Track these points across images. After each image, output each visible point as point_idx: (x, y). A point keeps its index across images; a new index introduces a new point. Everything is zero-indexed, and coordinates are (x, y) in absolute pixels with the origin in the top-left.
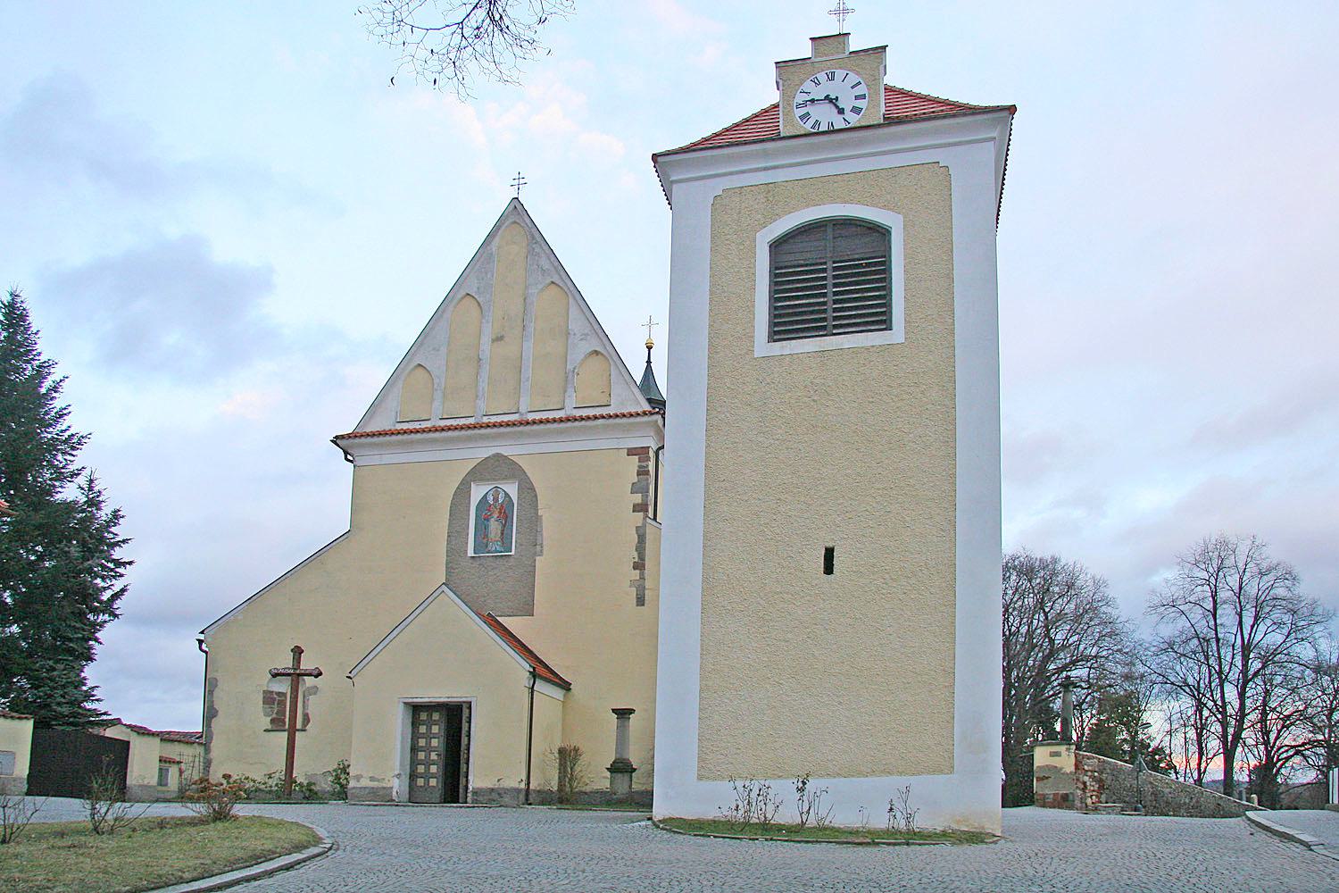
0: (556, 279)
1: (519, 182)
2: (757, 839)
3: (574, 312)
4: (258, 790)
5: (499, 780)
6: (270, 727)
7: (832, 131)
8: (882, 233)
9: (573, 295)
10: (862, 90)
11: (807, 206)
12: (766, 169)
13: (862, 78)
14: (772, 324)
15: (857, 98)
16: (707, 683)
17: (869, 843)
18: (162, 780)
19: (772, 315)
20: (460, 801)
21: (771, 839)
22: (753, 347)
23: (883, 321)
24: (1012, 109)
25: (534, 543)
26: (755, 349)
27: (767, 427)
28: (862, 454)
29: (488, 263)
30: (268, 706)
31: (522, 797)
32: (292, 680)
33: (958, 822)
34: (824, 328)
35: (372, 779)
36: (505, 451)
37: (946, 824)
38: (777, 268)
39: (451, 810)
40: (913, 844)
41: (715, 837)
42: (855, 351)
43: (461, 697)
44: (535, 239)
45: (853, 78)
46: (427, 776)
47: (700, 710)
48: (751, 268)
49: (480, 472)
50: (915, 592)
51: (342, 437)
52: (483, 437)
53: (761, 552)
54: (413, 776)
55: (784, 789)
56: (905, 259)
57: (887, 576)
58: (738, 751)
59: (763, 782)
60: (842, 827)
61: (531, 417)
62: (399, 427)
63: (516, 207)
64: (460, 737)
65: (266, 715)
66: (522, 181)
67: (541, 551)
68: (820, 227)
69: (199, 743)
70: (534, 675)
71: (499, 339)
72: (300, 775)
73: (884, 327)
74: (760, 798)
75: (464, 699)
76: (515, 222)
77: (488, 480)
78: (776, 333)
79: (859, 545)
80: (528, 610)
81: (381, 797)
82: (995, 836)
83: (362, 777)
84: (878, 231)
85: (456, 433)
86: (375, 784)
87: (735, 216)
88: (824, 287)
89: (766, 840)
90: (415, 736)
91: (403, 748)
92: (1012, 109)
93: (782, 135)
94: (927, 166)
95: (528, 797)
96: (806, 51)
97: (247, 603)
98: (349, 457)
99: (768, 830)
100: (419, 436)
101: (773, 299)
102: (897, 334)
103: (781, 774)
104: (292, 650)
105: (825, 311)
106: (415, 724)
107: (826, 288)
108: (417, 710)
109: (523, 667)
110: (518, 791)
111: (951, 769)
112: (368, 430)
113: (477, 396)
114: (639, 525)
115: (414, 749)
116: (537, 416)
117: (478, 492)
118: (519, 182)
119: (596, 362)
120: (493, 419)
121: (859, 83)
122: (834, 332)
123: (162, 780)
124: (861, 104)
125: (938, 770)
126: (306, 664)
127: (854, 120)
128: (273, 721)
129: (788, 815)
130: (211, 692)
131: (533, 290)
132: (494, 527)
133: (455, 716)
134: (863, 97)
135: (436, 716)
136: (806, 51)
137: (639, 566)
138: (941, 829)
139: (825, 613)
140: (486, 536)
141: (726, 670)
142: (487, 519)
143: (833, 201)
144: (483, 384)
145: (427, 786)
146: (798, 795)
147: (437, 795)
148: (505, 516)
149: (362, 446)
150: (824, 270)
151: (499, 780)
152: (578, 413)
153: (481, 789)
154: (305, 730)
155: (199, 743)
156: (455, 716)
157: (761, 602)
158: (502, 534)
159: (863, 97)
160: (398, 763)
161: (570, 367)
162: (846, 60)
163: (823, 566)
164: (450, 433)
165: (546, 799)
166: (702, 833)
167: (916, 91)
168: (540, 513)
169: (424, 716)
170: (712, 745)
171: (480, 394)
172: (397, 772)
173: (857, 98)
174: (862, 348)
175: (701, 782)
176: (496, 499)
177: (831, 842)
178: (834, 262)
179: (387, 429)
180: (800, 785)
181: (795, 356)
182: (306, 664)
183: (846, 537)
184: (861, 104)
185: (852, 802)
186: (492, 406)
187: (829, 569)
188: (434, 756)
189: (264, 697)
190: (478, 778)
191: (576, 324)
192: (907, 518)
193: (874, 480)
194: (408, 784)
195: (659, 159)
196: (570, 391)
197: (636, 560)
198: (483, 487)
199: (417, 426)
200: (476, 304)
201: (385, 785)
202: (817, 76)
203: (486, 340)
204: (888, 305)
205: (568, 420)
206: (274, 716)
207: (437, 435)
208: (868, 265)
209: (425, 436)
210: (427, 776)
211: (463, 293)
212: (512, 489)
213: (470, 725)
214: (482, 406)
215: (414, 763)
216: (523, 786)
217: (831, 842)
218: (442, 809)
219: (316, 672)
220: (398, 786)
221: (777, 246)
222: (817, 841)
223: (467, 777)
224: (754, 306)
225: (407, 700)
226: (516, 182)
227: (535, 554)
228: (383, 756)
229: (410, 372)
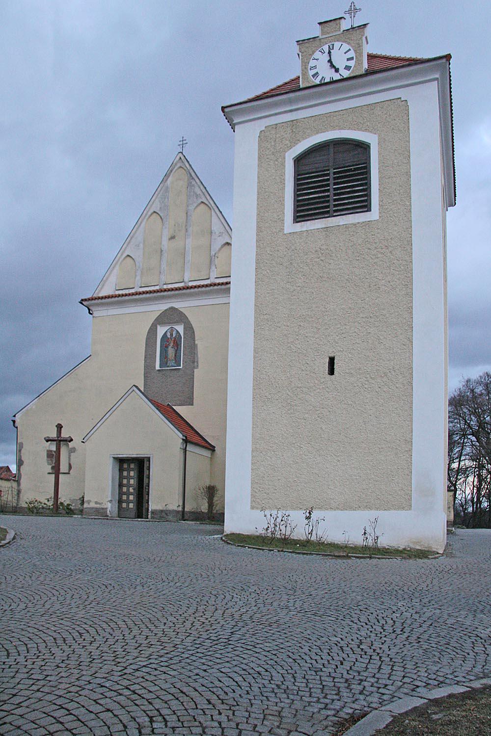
2: (273, 550)
3: (215, 219)
4: (43, 508)
5: (166, 505)
6: (51, 471)
7: (333, 82)
8: (363, 148)
9: (214, 210)
10: (352, 54)
11: (317, 133)
12: (291, 111)
13: (352, 47)
14: (296, 211)
15: (348, 60)
16: (256, 446)
17: (344, 556)
18: (452, 491)
19: (296, 206)
20: (144, 516)
21: (282, 551)
22: (284, 226)
23: (366, 206)
24: (448, 57)
25: (193, 362)
26: (285, 228)
27: (293, 278)
28: (352, 294)
29: (166, 193)
30: (49, 459)
31: (180, 516)
32: (57, 444)
33: (414, 543)
34: (328, 212)
35: (96, 503)
36: (176, 305)
37: (406, 544)
38: (299, 175)
39: (139, 523)
40: (374, 558)
41: (249, 547)
42: (346, 226)
43: (144, 455)
44: (192, 176)
45: (346, 47)
46: (128, 502)
47: (252, 464)
49: (162, 319)
50: (386, 387)
51: (86, 300)
52: (163, 297)
54: (120, 501)
55: (297, 517)
56: (379, 164)
57: (368, 376)
58: (275, 491)
59: (284, 512)
60: (339, 543)
61: (191, 284)
62: (117, 293)
63: (183, 159)
64: (143, 478)
65: (49, 464)
66: (184, 142)
67: (198, 366)
68: (325, 146)
69: (14, 480)
70: (186, 441)
71: (173, 238)
72: (64, 498)
73: (366, 210)
74: (282, 523)
75: (146, 456)
76: (181, 167)
77: (165, 323)
78: (298, 217)
79: (350, 355)
80: (189, 401)
81: (101, 513)
82: (438, 553)
83: (91, 501)
84: (362, 147)
85: (148, 295)
86: (98, 506)
87: (273, 144)
88: (328, 185)
89: (279, 551)
90: (121, 477)
91: (113, 486)
92: (448, 57)
93: (301, 87)
94: (393, 101)
95: (183, 515)
96: (317, 31)
97: (37, 399)
98: (91, 312)
99: (286, 544)
100: (127, 298)
101: (296, 195)
102: (374, 214)
103: (301, 507)
104: (56, 426)
105: (328, 201)
106: (121, 470)
107: (329, 186)
108: (122, 462)
109: (177, 437)
110: (178, 512)
111: (410, 507)
112: (100, 295)
113: (160, 272)
115: (121, 485)
116: (194, 284)
120: (170, 286)
121: (350, 50)
122: (334, 214)
123: (452, 491)
124: (352, 63)
125: (401, 508)
126: (64, 435)
127: (346, 74)
128: (52, 468)
129: (300, 533)
130: (20, 451)
131: (191, 208)
132: (171, 352)
133: (141, 465)
134: (352, 59)
135: (132, 466)
136: (317, 31)
138: (404, 547)
139: (329, 401)
140: (166, 357)
142: (167, 347)
143: (334, 128)
144: (164, 266)
145: (128, 508)
146: (307, 521)
147: (133, 514)
148: (177, 345)
149: (98, 305)
150: (328, 175)
151: (166, 505)
152: (217, 281)
153: (156, 510)
154: (69, 473)
155: (14, 480)
156: (141, 465)
157: (289, 393)
158: (175, 356)
159: (352, 59)
160: (110, 493)
161: (213, 253)
162: (342, 36)
163: (327, 369)
164: (144, 296)
165: (197, 516)
166: (242, 545)
167: (393, 55)
168: (196, 342)
169: (125, 466)
170: (260, 487)
171: (162, 272)
172: (110, 499)
173: (348, 60)
174: (352, 224)
175: (253, 510)
176: (172, 335)
177: (320, 555)
178: (334, 169)
179: (111, 294)
180: (308, 515)
181: (310, 232)
182: (64, 435)
183: (342, 350)
184: (352, 63)
185: (340, 526)
186: (169, 279)
187: (331, 371)
188: (131, 490)
189: (47, 454)
190: (154, 505)
192: (381, 337)
193: (359, 311)
194: (117, 506)
195: (226, 110)
196: (213, 268)
198: (164, 327)
199: (127, 292)
200: (159, 218)
201: (103, 507)
202: (323, 47)
204: (368, 195)
205: (211, 285)
206: (53, 465)
207: (137, 297)
208: (355, 170)
209: (130, 297)
210: (128, 502)
211: (151, 211)
212: (180, 328)
213: (149, 471)
214: (164, 279)
215: (121, 494)
216: (180, 509)
217: (320, 555)
218: (132, 522)
219: (69, 439)
220: (110, 507)
221: (298, 160)
222: (311, 554)
223: (148, 503)
224: (284, 200)
225: (114, 456)
227: (194, 368)
228: (98, 486)
229: (122, 261)
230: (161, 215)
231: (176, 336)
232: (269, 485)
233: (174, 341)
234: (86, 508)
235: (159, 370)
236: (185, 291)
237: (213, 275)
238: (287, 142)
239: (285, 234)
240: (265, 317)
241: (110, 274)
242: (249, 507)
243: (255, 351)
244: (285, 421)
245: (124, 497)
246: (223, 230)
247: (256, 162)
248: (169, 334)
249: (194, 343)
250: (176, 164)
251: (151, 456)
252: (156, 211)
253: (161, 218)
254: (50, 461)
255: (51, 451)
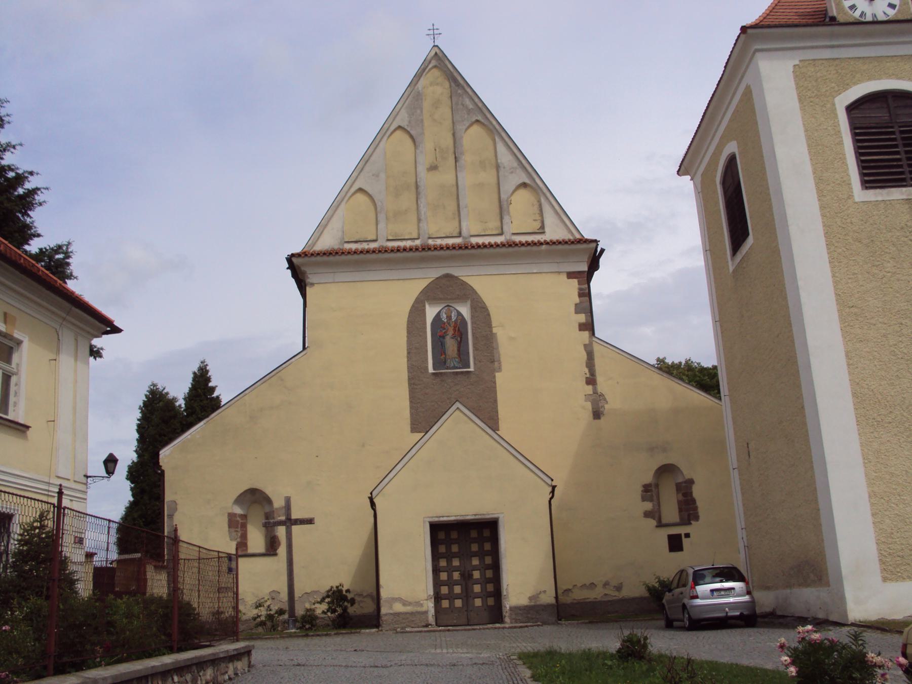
0: (480, 118)
1: (434, 33)
3: (501, 148)
44: (456, 81)
47: (873, 515)
48: (836, 125)
49: (429, 295)
51: (298, 255)
53: (895, 369)
66: (436, 32)
77: (441, 299)
78: (867, 182)
81: (409, 622)
110: (552, 605)
114: (587, 342)
117: (431, 312)
118: (434, 33)
119: (523, 194)
132: (451, 345)
137: (591, 381)
141: (888, 477)
142: (443, 337)
143: (890, 76)
168: (494, 330)
176: (449, 317)
179: (336, 247)
186: (439, 229)
191: (505, 157)
197: (588, 375)
203: (422, 170)
226: (431, 32)
228: (409, 579)
230: (412, 132)
231: (456, 320)
232: (902, 544)
233: (455, 327)
234: (386, 615)
235: (433, 374)
236: (467, 251)
237: (509, 229)
238: (833, 85)
239: (856, 203)
240: (852, 310)
241: (332, 216)
242: (880, 579)
243: (847, 356)
244: (907, 453)
245: (457, 589)
246: (515, 164)
247: (796, 104)
248: (445, 316)
249: (491, 331)
250: (430, 62)
251: (501, 516)
252: (402, 125)
253: (411, 137)
254: (234, 534)
255: (235, 515)
